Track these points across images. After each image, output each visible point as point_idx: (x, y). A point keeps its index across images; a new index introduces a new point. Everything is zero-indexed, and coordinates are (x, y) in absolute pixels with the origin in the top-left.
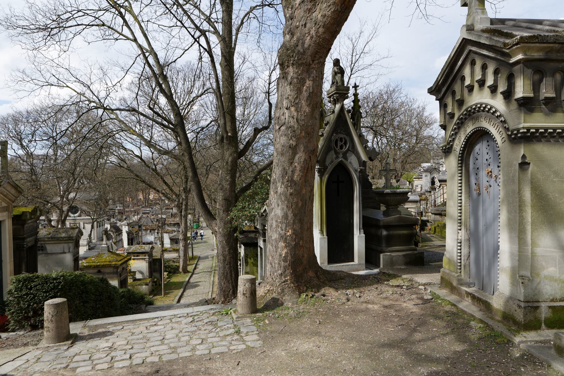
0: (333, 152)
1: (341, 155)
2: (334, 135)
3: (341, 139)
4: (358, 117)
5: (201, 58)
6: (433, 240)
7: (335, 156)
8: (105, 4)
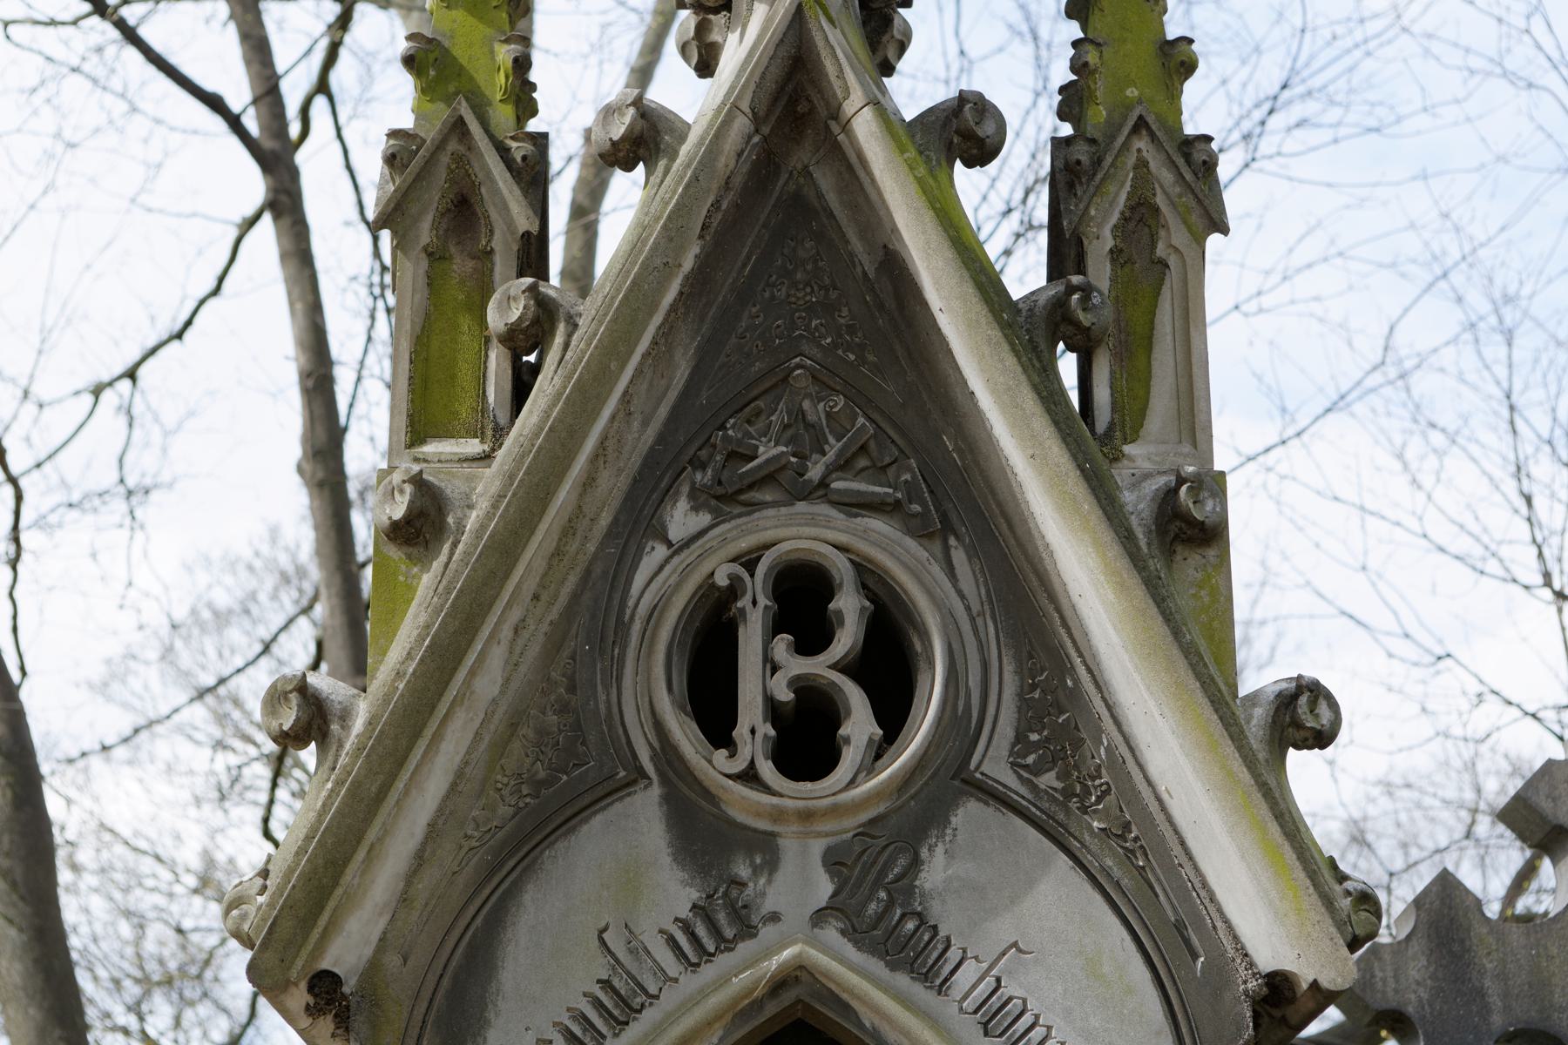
0: (642, 818)
1: (799, 884)
2: (681, 519)
3: (802, 602)
4: (1141, 216)
5: (1376, 16)
6: (654, 179)
7: (675, 894)
8: (613, 4)
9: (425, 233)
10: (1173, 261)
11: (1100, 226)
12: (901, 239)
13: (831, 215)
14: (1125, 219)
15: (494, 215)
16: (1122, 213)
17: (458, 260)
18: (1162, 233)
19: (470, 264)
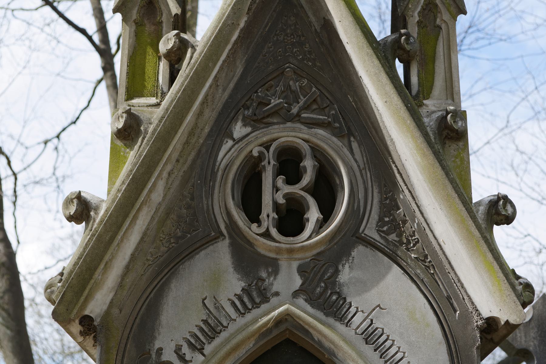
9: (134, 14)
10: (443, 26)
11: (413, 12)
12: (330, 14)
13: (302, 7)
14: (423, 9)
15: (163, 7)
16: (422, 7)
17: (148, 26)
18: (439, 15)
19: (153, 28)
